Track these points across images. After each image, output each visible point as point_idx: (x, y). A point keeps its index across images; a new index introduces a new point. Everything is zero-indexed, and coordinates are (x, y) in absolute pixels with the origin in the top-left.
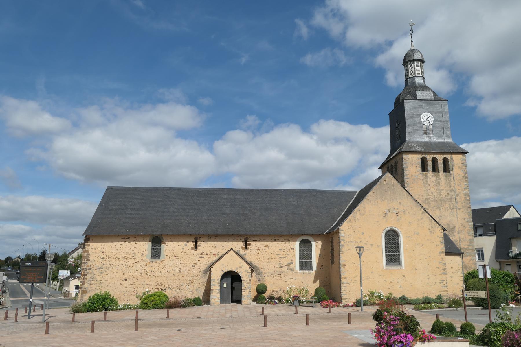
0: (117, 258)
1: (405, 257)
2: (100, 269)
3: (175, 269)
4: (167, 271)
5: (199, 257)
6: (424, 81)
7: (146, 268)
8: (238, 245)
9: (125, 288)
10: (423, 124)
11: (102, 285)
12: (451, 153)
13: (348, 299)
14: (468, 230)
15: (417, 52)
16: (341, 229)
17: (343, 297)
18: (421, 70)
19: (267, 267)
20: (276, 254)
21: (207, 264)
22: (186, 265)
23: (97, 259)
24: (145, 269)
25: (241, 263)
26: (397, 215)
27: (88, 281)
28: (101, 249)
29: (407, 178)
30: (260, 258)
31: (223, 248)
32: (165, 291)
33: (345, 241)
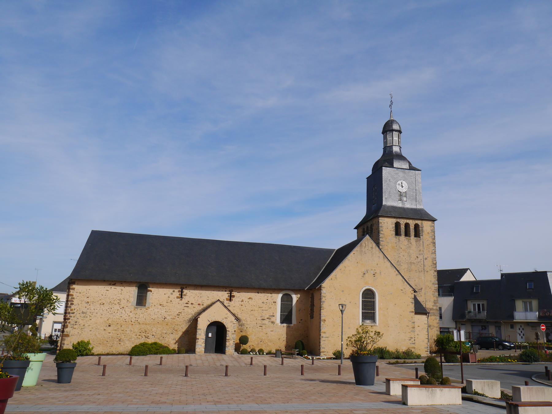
0: (102, 304)
1: (379, 315)
2: (84, 313)
3: (159, 317)
4: (152, 319)
5: (184, 306)
6: (400, 150)
7: (131, 314)
8: (223, 295)
9: (108, 334)
10: (398, 191)
11: (85, 329)
12: (422, 220)
13: (326, 352)
14: (433, 292)
15: (396, 123)
16: (323, 286)
17: (322, 350)
18: (398, 140)
19: (249, 318)
20: (259, 307)
21: (192, 313)
22: (170, 313)
23: (81, 303)
24: (130, 316)
25: (227, 314)
26: (374, 275)
27: (71, 325)
28: (86, 293)
29: (382, 241)
30: (243, 310)
31: (208, 298)
32: (149, 339)
33: (326, 298)
